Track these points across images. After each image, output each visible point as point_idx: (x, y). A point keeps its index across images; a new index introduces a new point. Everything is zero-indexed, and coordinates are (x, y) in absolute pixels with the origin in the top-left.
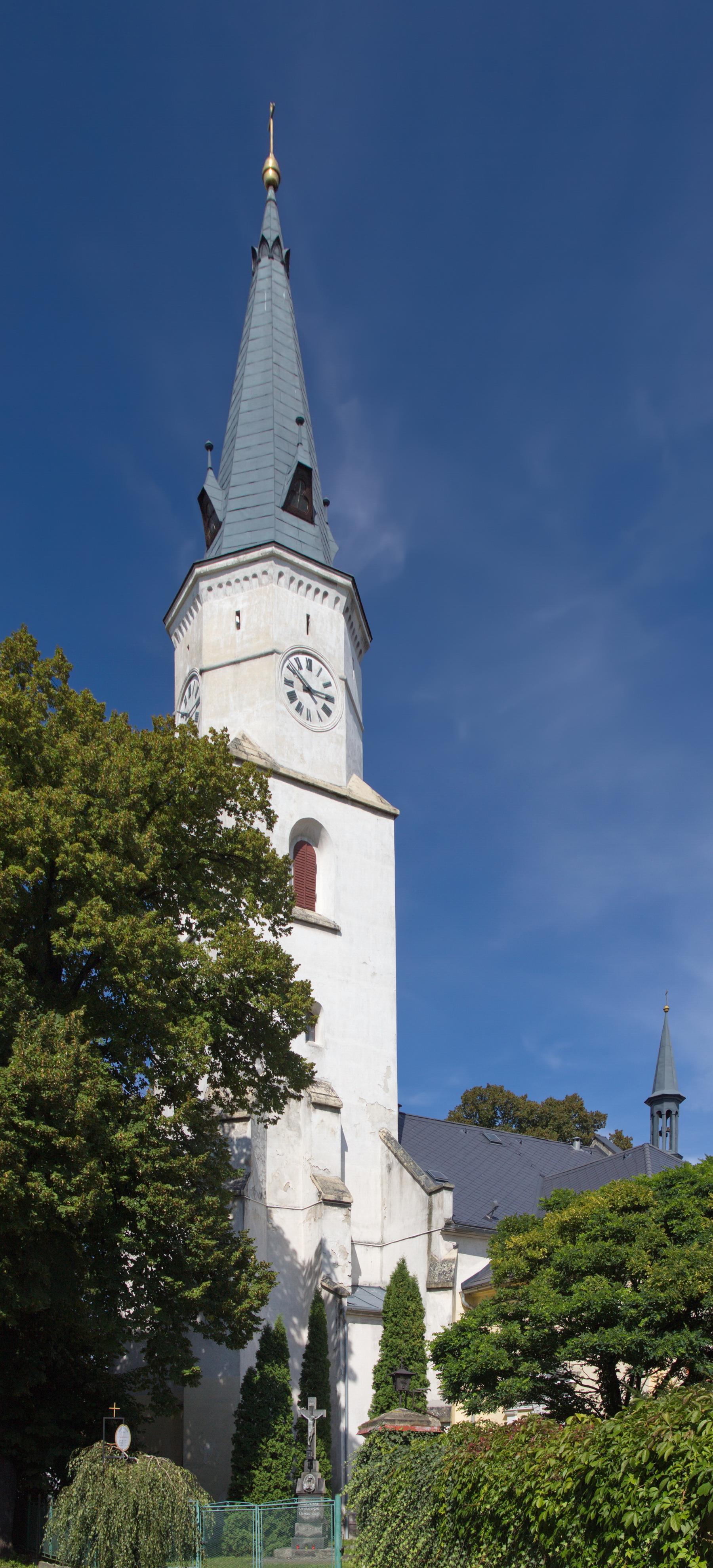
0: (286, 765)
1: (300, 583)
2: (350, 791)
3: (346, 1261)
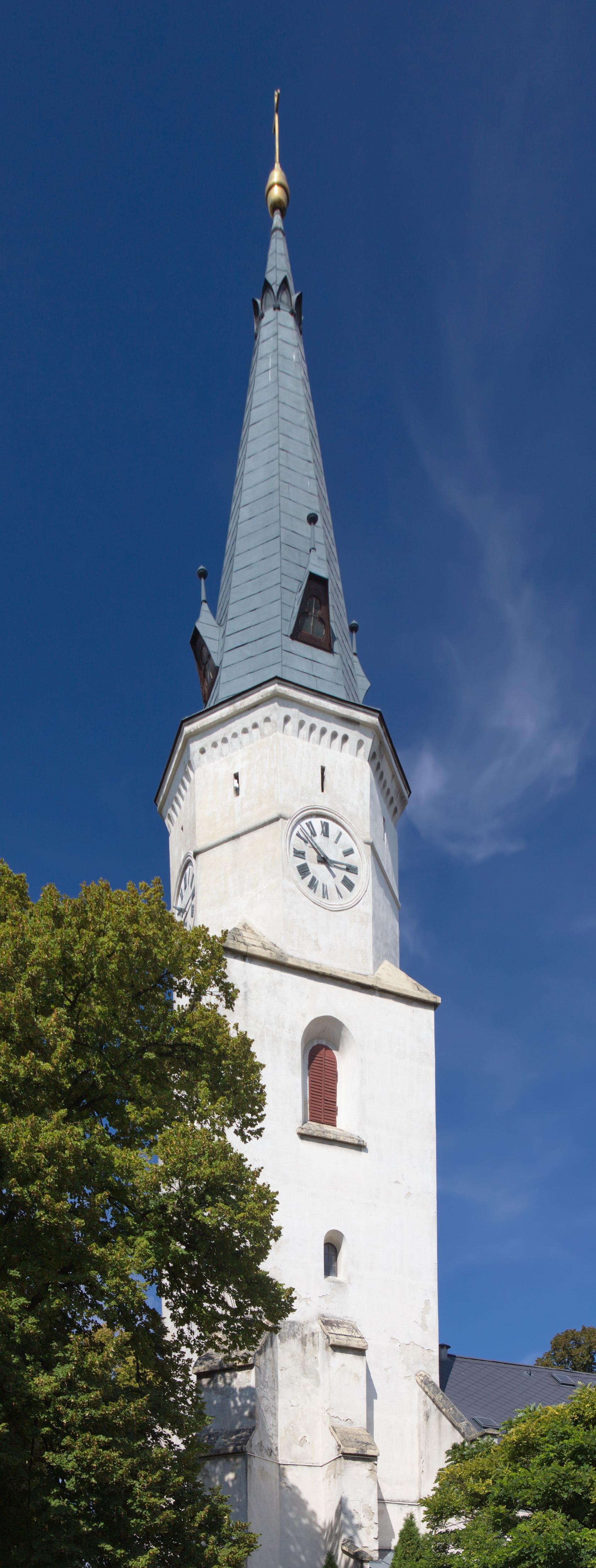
0: (297, 955)
1: (312, 728)
2: (378, 979)
3: (372, 1522)
